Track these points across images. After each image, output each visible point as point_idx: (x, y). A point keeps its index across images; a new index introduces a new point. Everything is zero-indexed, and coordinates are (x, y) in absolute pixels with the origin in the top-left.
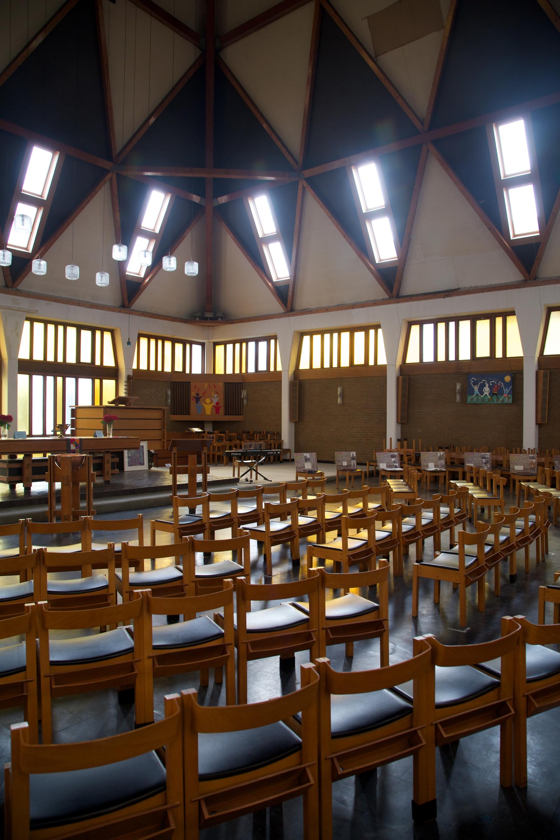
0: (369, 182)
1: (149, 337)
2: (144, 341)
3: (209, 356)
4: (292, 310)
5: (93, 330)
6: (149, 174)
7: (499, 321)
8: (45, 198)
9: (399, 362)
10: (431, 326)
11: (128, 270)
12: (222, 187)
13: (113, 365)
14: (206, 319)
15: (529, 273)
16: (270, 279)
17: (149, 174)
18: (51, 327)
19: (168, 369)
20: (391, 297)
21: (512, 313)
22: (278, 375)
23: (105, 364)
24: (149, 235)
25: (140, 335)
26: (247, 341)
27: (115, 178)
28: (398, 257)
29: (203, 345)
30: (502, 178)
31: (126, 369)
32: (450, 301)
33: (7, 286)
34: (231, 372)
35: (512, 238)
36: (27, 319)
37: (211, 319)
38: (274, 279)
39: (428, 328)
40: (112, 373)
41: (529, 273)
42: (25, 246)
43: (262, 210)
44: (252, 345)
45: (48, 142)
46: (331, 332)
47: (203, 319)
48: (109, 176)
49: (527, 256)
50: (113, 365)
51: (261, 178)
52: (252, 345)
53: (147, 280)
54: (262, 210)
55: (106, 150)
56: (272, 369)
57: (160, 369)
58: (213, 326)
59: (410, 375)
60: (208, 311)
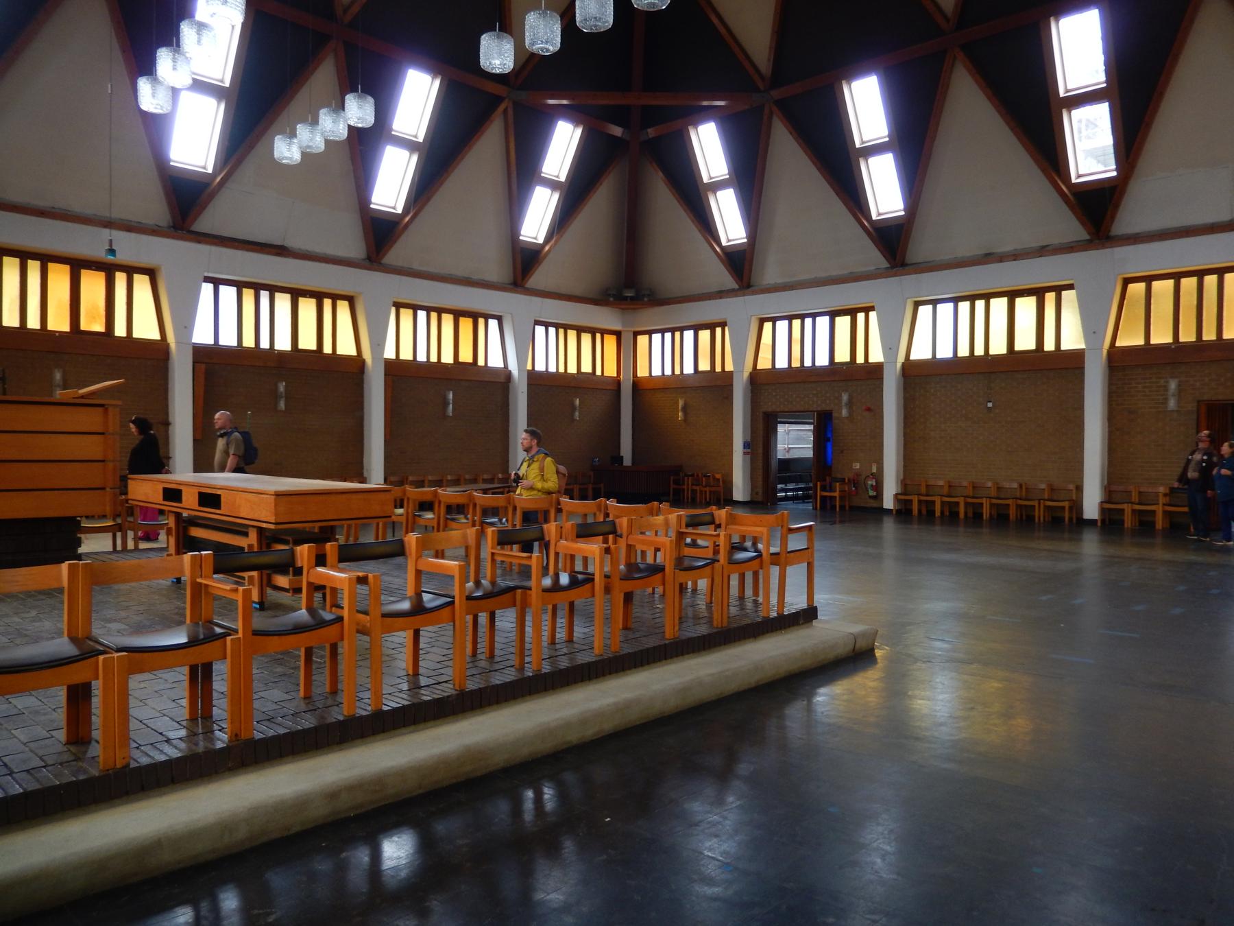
1: (547, 325)
4: (749, 286)
5: (319, 297)
6: (551, 102)
9: (901, 358)
10: (1004, 301)
11: (373, 200)
12: (651, 116)
13: (353, 353)
14: (626, 298)
16: (719, 242)
17: (551, 102)
19: (448, 358)
20: (892, 267)
21: (1070, 287)
22: (727, 377)
23: (340, 351)
24: (553, 185)
26: (682, 330)
27: (510, 112)
28: (905, 210)
29: (618, 334)
30: (1062, 94)
31: (373, 358)
32: (983, 269)
33: (369, 258)
35: (1074, 181)
36: (208, 280)
38: (724, 243)
43: (709, 147)
48: (502, 107)
50: (353, 353)
51: (705, 103)
52: (689, 335)
53: (407, 219)
54: (709, 147)
56: (718, 369)
59: (918, 376)
60: (630, 289)
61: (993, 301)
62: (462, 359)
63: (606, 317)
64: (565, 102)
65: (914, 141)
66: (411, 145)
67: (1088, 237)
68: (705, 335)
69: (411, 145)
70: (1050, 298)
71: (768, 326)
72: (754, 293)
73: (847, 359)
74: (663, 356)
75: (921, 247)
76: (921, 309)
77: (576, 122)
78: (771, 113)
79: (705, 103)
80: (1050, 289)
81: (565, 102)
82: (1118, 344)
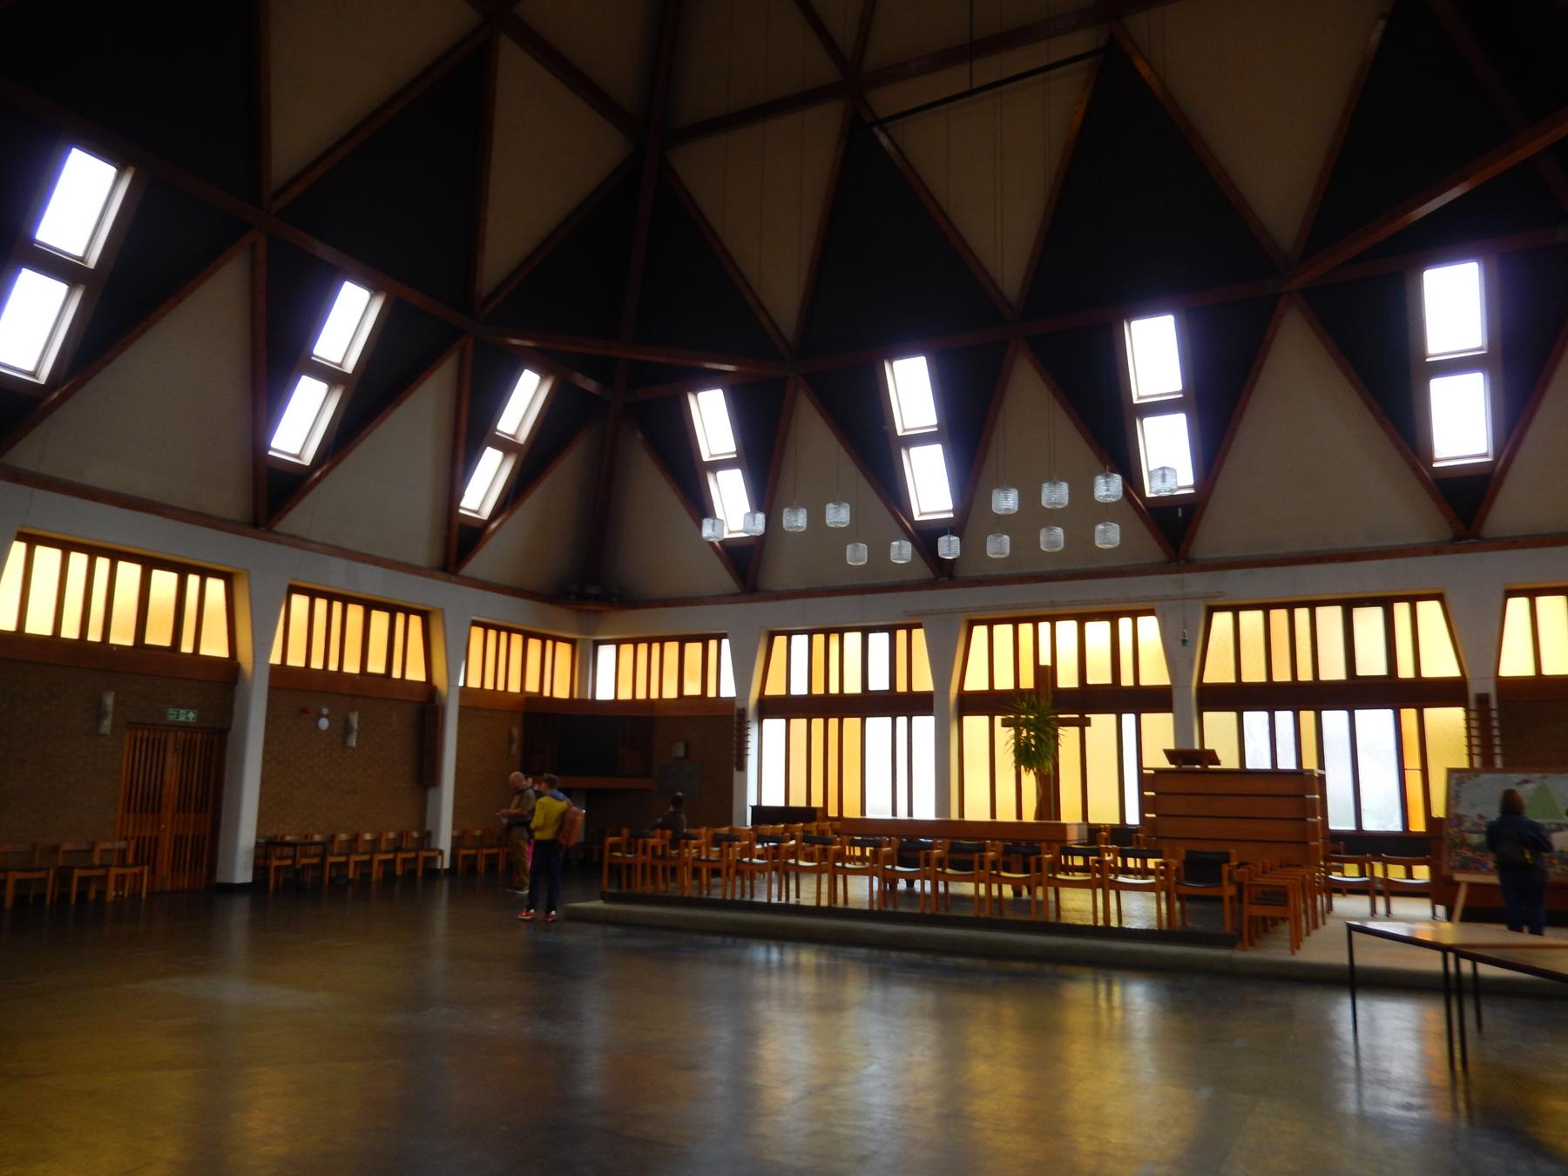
1: (313, 594)
2: (299, 603)
3: (584, 665)
6: (516, 342)
7: (713, 644)
8: (92, 262)
11: (273, 444)
17: (516, 342)
18: (321, 604)
19: (352, 667)
21: (919, 626)
24: (506, 446)
25: (294, 589)
26: (662, 641)
34: (814, 721)
36: (21, 537)
42: (31, 368)
43: (712, 419)
45: (543, 371)
46: (649, 642)
51: (709, 365)
53: (493, 526)
54: (712, 419)
57: (501, 687)
60: (589, 584)
61: (794, 638)
62: (371, 668)
65: (1215, 402)
67: (932, 576)
68: (694, 650)
70: (901, 635)
71: (780, 641)
73: (886, 687)
74: (615, 675)
75: (1210, 539)
79: (709, 365)
80: (901, 627)
82: (767, 693)
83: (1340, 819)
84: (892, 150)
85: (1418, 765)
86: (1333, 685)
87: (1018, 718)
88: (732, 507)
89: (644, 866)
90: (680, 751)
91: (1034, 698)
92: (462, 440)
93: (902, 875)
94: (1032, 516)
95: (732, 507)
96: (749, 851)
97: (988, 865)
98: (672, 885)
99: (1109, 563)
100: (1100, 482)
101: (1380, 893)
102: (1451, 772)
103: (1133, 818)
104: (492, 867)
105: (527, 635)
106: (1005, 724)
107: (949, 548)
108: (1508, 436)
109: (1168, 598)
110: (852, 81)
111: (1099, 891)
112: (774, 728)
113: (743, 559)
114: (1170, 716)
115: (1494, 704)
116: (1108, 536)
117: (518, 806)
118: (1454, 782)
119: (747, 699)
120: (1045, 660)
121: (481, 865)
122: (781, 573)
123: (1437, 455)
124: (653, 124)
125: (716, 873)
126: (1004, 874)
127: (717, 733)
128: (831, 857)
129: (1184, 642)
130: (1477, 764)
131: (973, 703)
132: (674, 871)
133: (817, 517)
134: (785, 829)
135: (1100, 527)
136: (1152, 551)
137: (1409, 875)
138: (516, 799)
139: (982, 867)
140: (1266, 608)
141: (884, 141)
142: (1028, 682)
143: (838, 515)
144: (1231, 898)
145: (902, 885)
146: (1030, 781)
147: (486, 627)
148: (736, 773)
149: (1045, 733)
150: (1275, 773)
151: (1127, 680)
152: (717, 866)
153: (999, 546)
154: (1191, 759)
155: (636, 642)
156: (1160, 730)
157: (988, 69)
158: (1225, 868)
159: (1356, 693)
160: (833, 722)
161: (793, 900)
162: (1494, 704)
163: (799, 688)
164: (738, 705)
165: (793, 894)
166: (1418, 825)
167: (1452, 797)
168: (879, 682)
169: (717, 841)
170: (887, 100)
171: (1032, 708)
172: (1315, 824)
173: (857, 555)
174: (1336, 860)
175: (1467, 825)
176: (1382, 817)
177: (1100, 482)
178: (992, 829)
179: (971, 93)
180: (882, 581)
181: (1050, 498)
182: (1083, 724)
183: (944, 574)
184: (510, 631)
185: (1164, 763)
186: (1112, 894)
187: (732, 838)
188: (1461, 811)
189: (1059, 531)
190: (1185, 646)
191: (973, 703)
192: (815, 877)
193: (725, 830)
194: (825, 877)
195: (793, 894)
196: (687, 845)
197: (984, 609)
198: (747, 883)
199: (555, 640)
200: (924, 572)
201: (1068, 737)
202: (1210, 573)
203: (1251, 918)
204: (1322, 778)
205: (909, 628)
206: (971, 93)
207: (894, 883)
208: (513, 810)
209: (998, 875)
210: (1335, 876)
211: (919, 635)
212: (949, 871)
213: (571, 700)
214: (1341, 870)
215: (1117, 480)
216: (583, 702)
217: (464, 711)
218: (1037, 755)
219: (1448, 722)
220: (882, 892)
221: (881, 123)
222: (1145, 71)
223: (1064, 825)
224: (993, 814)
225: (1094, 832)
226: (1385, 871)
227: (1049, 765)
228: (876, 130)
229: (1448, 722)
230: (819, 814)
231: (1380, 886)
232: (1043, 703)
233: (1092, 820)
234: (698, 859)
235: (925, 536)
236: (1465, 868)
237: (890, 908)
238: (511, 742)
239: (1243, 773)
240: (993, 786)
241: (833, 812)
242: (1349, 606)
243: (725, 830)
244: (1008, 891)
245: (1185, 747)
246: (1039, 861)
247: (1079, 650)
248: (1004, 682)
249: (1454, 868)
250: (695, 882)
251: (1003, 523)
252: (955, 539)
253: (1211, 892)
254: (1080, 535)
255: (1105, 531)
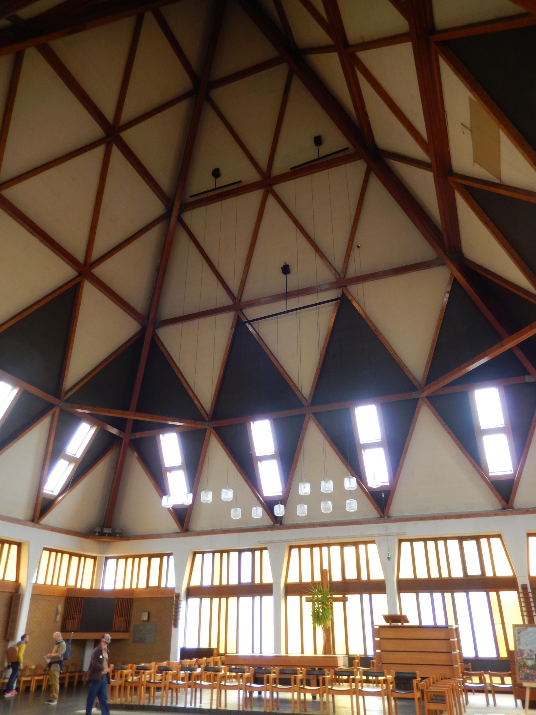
0: (262, 434)
6: (80, 411)
10: (146, 559)
12: (138, 426)
15: (383, 511)
21: (373, 542)
24: (71, 459)
26: (140, 557)
37: (110, 535)
39: (208, 557)
40: (509, 584)
41: (383, 511)
43: (170, 446)
44: (145, 560)
46: (134, 557)
47: (102, 534)
48: (53, 411)
49: (505, 492)
51: (170, 423)
52: (234, 555)
53: (60, 498)
54: (170, 446)
55: (56, 390)
58: (108, 542)
60: (106, 528)
63: (90, 546)
64: (87, 412)
66: (171, 469)
68: (156, 561)
69: (171, 469)
70: (257, 553)
71: (199, 557)
72: (190, 535)
76: (403, 544)
77: (92, 423)
78: (211, 433)
79: (170, 423)
81: (87, 412)
83: (468, 652)
84: (254, 333)
85: (500, 622)
86: (457, 580)
87: (313, 597)
88: (178, 491)
89: (120, 687)
90: (145, 617)
91: (321, 586)
92: (49, 456)
93: (255, 689)
94: (317, 496)
95: (178, 491)
96: (176, 677)
97: (298, 682)
98: (135, 697)
99: (353, 518)
100: (346, 480)
101: (490, 692)
102: (515, 626)
103: (370, 652)
104: (39, 688)
105: (71, 555)
106: (308, 600)
107: (279, 510)
108: (518, 463)
109: (380, 535)
110: (237, 305)
111: (354, 696)
112: (194, 602)
113: (183, 517)
114: (385, 595)
115: (529, 590)
116: (352, 506)
117: (56, 652)
118: (516, 632)
119: (181, 588)
120: (326, 567)
121: (33, 688)
122: (199, 522)
123: (490, 471)
124: (150, 321)
125: (158, 689)
126: (306, 687)
127: (163, 606)
128: (218, 679)
129: (389, 558)
130: (527, 623)
131: (291, 589)
132: (136, 688)
133: (217, 495)
134: (197, 661)
135: (348, 501)
136: (372, 512)
137: (503, 683)
138: (56, 647)
139: (295, 684)
140: (425, 540)
141: (251, 329)
142: (318, 578)
143: (227, 495)
144: (419, 699)
145: (256, 694)
146: (320, 630)
147: (51, 550)
148: (173, 629)
149: (327, 605)
150: (435, 628)
151: (364, 577)
152: (158, 686)
153: (302, 510)
154: (395, 620)
155: (126, 558)
156: (381, 604)
157: (293, 303)
158: (415, 682)
159: (468, 584)
160: (224, 600)
161: (198, 706)
162: (529, 590)
163: (207, 583)
164: (176, 591)
165: (198, 701)
166: (504, 654)
167: (517, 641)
168: (246, 579)
169: (160, 670)
170: (251, 313)
171: (320, 592)
172: (456, 655)
173: (236, 514)
174: (467, 674)
175: (525, 655)
176: (487, 652)
177: (346, 480)
178: (301, 661)
179: (287, 312)
180: (249, 526)
181: (325, 488)
182: (344, 600)
183: (278, 523)
184: (63, 553)
185: (384, 623)
186: (361, 698)
187: (167, 669)
188: (522, 648)
189: (330, 503)
190: (390, 560)
191: (291, 589)
192: (210, 690)
193: (164, 664)
194: (215, 691)
195: (198, 701)
196: (144, 673)
197: (296, 540)
198: (175, 694)
199: (86, 557)
200: (269, 522)
201: (337, 606)
202: (399, 523)
203: (429, 710)
204: (457, 630)
205: (261, 550)
206: (287, 312)
207: (251, 693)
208: (53, 654)
209: (303, 688)
210: (468, 684)
211: (265, 553)
212: (279, 686)
213: (91, 590)
214: (471, 679)
215: (354, 480)
216: (97, 591)
217: (34, 597)
218: (321, 617)
219: (510, 599)
220: (246, 699)
221: (249, 322)
222: (357, 306)
223: (336, 657)
224: (302, 653)
225: (351, 660)
226: (491, 680)
227: (329, 623)
228: (247, 324)
229: (510, 599)
230: (215, 652)
231: (489, 688)
232: (325, 589)
233: (351, 653)
234: (149, 682)
235: (269, 506)
236: (527, 679)
237: (249, 709)
238: (57, 613)
239: (420, 627)
240: (301, 639)
241: (222, 651)
242: (461, 539)
243: (164, 664)
244: (309, 697)
245: (393, 613)
246: (324, 679)
247: (341, 562)
248: (307, 579)
249: (522, 679)
250: (147, 695)
251: (304, 499)
252: (282, 507)
253: (409, 696)
254: (339, 506)
255: (350, 503)
